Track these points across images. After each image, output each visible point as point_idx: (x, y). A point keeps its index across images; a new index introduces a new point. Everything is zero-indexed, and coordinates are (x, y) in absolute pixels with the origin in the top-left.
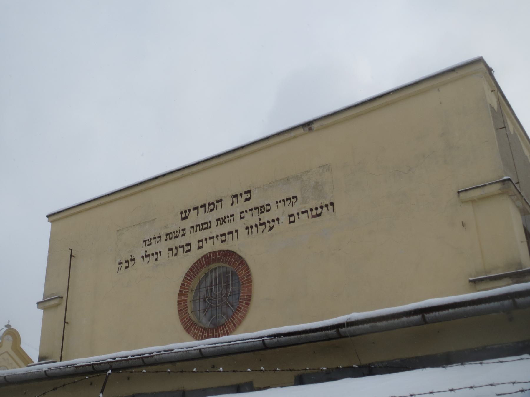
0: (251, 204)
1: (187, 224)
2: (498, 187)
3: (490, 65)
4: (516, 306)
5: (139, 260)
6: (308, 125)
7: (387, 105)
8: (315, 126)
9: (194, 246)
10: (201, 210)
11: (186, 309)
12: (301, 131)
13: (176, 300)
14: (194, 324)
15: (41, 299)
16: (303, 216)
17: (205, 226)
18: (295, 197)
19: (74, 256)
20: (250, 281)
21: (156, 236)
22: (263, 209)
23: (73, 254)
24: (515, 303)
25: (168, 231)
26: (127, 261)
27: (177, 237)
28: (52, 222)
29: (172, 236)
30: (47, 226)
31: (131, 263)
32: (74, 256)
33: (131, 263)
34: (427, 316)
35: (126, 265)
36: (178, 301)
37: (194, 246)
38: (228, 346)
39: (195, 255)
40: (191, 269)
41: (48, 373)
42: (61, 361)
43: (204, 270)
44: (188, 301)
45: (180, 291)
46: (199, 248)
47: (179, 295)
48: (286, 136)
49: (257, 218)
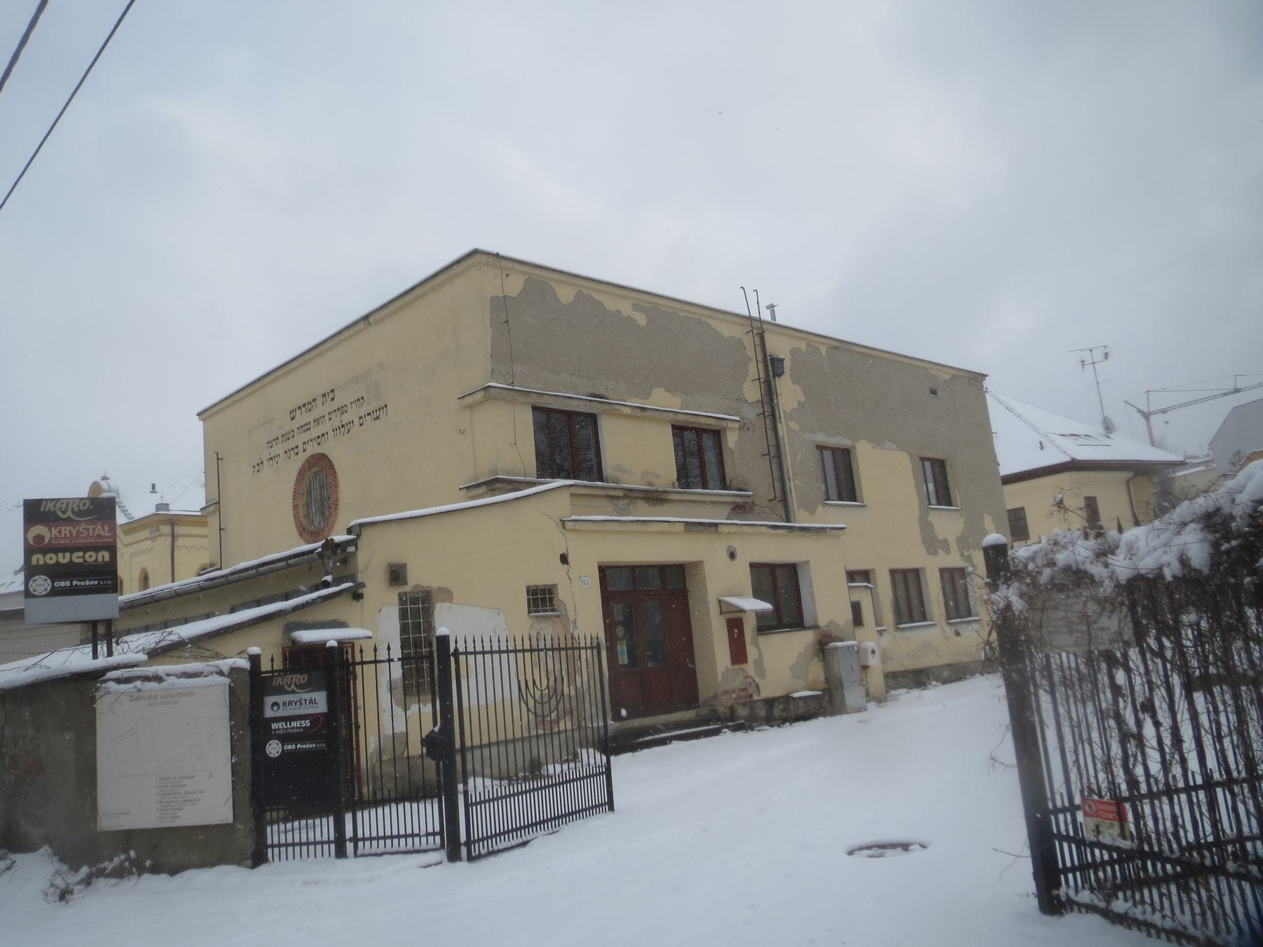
0: (336, 405)
1: (295, 425)
2: (482, 393)
3: (494, 250)
4: (289, 566)
5: (266, 463)
6: (366, 318)
7: (420, 297)
8: (371, 319)
9: (300, 449)
10: (303, 409)
11: (769, 358)
12: (362, 325)
13: (291, 505)
14: (304, 529)
15: (204, 505)
16: (368, 418)
17: (307, 427)
18: (362, 398)
19: (221, 459)
20: (336, 486)
21: (336, 409)
22: (342, 410)
23: (220, 457)
24: (287, 563)
25: (283, 432)
26: (258, 465)
27: (289, 439)
28: (204, 420)
29: (287, 437)
30: (200, 424)
31: (261, 466)
32: (221, 459)
33: (261, 466)
34: (289, 562)
35: (257, 468)
36: (293, 506)
37: (300, 449)
38: (211, 582)
39: (303, 457)
40: (299, 474)
41: (177, 591)
42: (173, 581)
43: (308, 474)
44: (300, 506)
45: (294, 496)
46: (304, 450)
47: (294, 499)
48: (407, 299)
49: (339, 419)
